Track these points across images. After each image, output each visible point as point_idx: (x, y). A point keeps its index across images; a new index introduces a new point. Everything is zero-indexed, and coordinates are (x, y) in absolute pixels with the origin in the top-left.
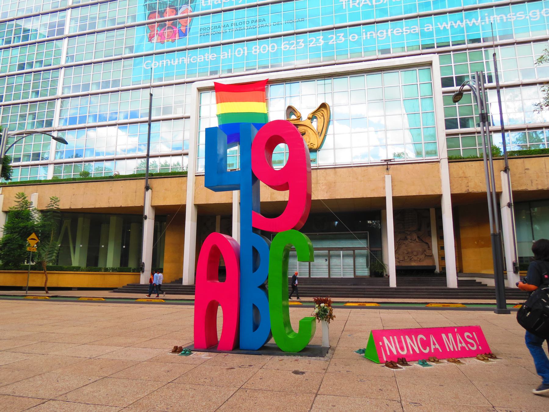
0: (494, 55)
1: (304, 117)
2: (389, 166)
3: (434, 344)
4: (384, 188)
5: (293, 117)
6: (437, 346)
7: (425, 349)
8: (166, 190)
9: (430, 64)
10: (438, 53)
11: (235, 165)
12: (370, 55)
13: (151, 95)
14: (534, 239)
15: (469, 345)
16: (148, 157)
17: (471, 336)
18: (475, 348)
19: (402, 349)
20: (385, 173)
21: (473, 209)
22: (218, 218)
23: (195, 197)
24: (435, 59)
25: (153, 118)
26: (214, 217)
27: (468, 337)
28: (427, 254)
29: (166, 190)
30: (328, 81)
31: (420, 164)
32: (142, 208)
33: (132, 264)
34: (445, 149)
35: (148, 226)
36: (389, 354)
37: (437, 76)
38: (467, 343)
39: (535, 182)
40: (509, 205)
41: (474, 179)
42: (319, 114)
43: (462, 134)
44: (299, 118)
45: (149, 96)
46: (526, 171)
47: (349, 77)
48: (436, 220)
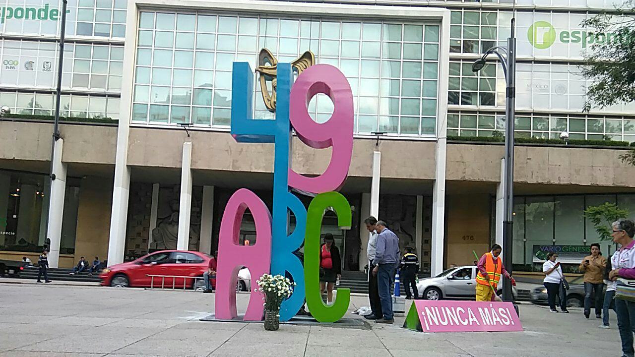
0: (513, 20)
2: (379, 141)
3: (472, 317)
4: (372, 167)
5: (267, 65)
6: (475, 319)
7: (464, 321)
9: (439, 20)
10: (448, 8)
11: (186, 119)
14: (525, 238)
15: (503, 320)
16: (59, 92)
17: (505, 312)
18: (508, 323)
19: (444, 321)
22: (156, 187)
24: (446, 14)
25: (66, 37)
27: (502, 312)
29: (85, 141)
30: (315, 24)
32: (49, 164)
35: (57, 190)
36: (431, 324)
37: (446, 40)
38: (501, 317)
39: (535, 174)
41: (481, 164)
42: (300, 66)
46: (528, 161)
47: (341, 21)
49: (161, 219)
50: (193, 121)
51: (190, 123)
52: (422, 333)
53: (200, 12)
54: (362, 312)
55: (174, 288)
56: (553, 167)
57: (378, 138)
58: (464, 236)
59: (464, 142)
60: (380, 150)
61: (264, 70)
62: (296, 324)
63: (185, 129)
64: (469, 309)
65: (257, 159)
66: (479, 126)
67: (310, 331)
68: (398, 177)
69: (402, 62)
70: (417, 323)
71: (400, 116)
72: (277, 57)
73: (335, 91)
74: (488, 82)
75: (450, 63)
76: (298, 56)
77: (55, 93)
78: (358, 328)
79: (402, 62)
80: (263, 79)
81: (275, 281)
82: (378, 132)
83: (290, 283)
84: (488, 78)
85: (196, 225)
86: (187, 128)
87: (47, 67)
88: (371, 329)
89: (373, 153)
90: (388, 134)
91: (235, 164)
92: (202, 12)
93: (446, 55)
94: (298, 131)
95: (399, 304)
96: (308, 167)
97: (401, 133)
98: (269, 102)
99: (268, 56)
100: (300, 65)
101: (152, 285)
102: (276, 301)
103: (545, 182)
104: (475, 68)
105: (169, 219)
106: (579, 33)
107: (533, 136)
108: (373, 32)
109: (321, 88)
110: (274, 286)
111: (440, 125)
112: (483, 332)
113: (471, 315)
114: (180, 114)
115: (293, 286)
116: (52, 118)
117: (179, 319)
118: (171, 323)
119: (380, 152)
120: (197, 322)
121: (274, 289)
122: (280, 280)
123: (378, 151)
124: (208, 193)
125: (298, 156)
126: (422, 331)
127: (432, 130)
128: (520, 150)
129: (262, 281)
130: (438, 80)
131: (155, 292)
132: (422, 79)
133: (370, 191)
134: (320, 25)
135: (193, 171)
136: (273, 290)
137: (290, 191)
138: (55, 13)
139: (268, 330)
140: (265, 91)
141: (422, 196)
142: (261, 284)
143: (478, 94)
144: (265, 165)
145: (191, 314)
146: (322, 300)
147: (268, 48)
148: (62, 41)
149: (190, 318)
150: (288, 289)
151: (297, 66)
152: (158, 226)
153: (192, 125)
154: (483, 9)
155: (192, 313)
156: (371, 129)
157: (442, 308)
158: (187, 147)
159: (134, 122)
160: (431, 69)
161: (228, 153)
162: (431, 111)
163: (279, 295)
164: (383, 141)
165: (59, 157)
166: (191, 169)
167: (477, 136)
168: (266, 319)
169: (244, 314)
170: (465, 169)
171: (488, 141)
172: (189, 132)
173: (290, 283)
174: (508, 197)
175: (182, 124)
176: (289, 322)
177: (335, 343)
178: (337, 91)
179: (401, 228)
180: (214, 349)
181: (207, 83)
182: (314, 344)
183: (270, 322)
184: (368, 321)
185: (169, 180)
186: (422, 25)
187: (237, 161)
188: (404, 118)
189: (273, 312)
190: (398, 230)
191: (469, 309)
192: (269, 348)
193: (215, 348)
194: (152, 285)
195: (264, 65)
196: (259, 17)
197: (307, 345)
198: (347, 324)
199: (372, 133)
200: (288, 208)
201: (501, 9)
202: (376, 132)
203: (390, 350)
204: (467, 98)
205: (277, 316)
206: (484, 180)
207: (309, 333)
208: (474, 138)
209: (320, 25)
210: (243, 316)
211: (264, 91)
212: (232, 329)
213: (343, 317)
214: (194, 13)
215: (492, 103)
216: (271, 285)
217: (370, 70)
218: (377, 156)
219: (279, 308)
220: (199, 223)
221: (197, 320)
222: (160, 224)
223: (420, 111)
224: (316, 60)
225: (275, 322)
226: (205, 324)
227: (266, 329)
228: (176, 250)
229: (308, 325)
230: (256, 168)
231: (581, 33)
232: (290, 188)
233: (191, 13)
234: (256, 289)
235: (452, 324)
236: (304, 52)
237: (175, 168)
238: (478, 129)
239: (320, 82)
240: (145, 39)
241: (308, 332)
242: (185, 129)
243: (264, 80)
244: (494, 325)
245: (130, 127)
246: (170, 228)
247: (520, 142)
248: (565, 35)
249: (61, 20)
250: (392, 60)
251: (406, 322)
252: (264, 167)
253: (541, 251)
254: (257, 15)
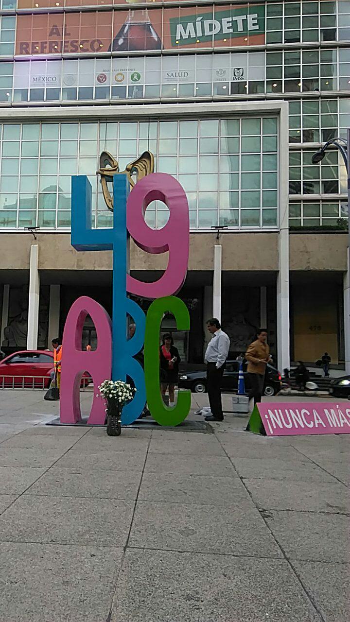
1: (122, 169)
2: (220, 234)
3: (318, 419)
4: (213, 261)
5: (108, 167)
6: (321, 421)
9: (277, 112)
10: (286, 99)
12: (83, 113)
19: (288, 424)
20: (215, 243)
22: (7, 287)
24: (284, 106)
30: (154, 125)
36: (275, 427)
42: (139, 166)
43: (305, 201)
44: (116, 168)
49: (12, 318)
50: (39, 224)
51: (37, 226)
52: (266, 437)
53: (43, 121)
54: (204, 413)
55: (23, 387)
57: (218, 233)
59: (308, 232)
60: (220, 243)
61: (105, 172)
62: (139, 428)
63: (32, 233)
64: (314, 411)
65: (99, 261)
66: (322, 214)
67: (151, 435)
68: (240, 270)
69: (240, 156)
70: (261, 427)
71: (240, 209)
72: (117, 159)
73: (169, 198)
74: (333, 170)
75: (289, 153)
78: (200, 432)
79: (240, 156)
81: (116, 388)
82: (218, 225)
83: (130, 388)
84: (332, 166)
85: (44, 323)
86: (34, 231)
88: (213, 433)
89: (214, 247)
90: (228, 228)
91: (79, 263)
92: (45, 121)
93: (285, 146)
94: (135, 239)
95: (243, 405)
96: (149, 263)
97: (241, 226)
98: (111, 202)
99: (108, 159)
100: (139, 165)
101: (3, 385)
102: (117, 406)
104: (315, 160)
105: (20, 317)
108: (211, 127)
109: (157, 195)
110: (115, 392)
111: (282, 216)
112: (329, 435)
113: (317, 417)
115: (134, 392)
117: (27, 424)
118: (20, 428)
119: (221, 246)
120: (43, 426)
121: (115, 395)
122: (121, 386)
123: (219, 244)
124: (55, 290)
125: (139, 253)
126: (265, 435)
127: (272, 221)
129: (103, 387)
131: (6, 392)
132: (261, 171)
133: (212, 284)
134: (158, 125)
135: (40, 272)
136: (114, 397)
137: (129, 296)
139: (111, 435)
140: (106, 192)
141: (266, 288)
142: (102, 390)
143: (321, 183)
144: (107, 263)
145: (38, 417)
146: (163, 402)
147: (108, 151)
149: (36, 422)
150: (128, 394)
151: (136, 167)
152: (9, 324)
153: (38, 229)
154: (323, 97)
155: (38, 416)
156: (212, 223)
157: (286, 411)
158: (34, 249)
160: (271, 159)
161: (73, 253)
162: (272, 201)
163: (120, 401)
164: (223, 234)
166: (38, 270)
167: (321, 225)
168: (108, 422)
169: (89, 416)
170: (309, 259)
171: (332, 230)
172: (35, 235)
173: (130, 388)
175: (29, 228)
176: (131, 426)
177: (176, 450)
178: (171, 198)
179: (245, 319)
180: (57, 458)
181: (52, 185)
182: (155, 451)
183: (113, 428)
184: (211, 423)
186: (260, 119)
187: (81, 261)
189: (114, 418)
190: (242, 322)
191: (314, 411)
192: (111, 457)
193: (59, 458)
194: (3, 385)
195: (105, 168)
196: (98, 122)
197: (147, 452)
198: (189, 427)
199: (212, 227)
200: (128, 315)
202: (216, 226)
203: (232, 458)
204: (309, 187)
205: (119, 421)
206: (330, 270)
207: (151, 438)
208: (318, 227)
209: (158, 125)
210: (86, 419)
211: (105, 192)
212: (76, 434)
213: (186, 419)
214: (38, 123)
216: (112, 391)
217: (209, 165)
218: (218, 249)
219: (120, 413)
220: (47, 321)
221: (43, 425)
222: (10, 323)
223: (260, 203)
224: (155, 158)
225: (117, 427)
226: (51, 428)
227: (109, 435)
228: (26, 349)
229: (149, 428)
230: (99, 267)
232: (128, 293)
233: (34, 123)
234: (97, 395)
235: (297, 427)
237: (24, 269)
238: (321, 218)
239: (155, 190)
241: (149, 437)
242: (32, 233)
243: (105, 181)
244: (341, 427)
246: (20, 326)
250: (232, 155)
251: (248, 425)
252: (107, 264)
254: (97, 120)
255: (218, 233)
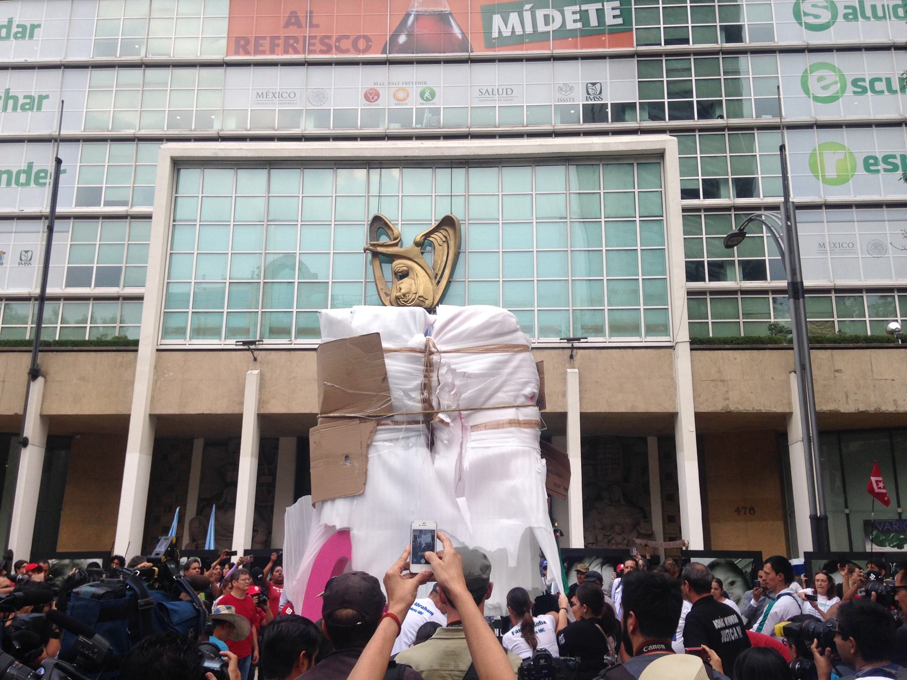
4: (564, 395)
5: (384, 239)
8: (82, 379)
9: (659, 156)
10: (673, 131)
11: (251, 333)
13: (59, 162)
14: (847, 507)
20: (567, 365)
21: (743, 449)
22: (199, 444)
23: (153, 397)
24: (669, 143)
25: (60, 210)
26: (644, 441)
28: (642, 531)
29: (82, 379)
30: (459, 173)
31: (635, 351)
33: (676, 113)
34: (686, 321)
37: (673, 177)
40: (25, 443)
41: (758, 384)
44: (397, 241)
45: (54, 164)
46: (837, 374)
48: (660, 462)
56: (882, 382)
58: (738, 508)
76: (433, 222)
77: (36, 299)
80: (377, 263)
86: (253, 347)
87: (25, 259)
89: (566, 373)
90: (590, 339)
93: (675, 203)
103: (872, 409)
104: (729, 243)
106: (894, 157)
107: (839, 331)
108: (554, 179)
114: (240, 322)
116: (28, 343)
119: (576, 370)
127: (663, 328)
128: (820, 358)
130: (666, 247)
132: (639, 248)
138: (42, 174)
148: (52, 219)
159: (164, 342)
162: (658, 295)
164: (581, 351)
165: (34, 410)
174: (809, 440)
185: (221, 434)
188: (615, 312)
201: (762, 128)
204: (712, 188)
208: (737, 339)
215: (739, 39)
231: (898, 157)
236: (443, 216)
240: (186, 209)
245: (158, 350)
247: (821, 342)
248: (871, 161)
249: (51, 186)
253: (878, 530)
255: (572, 348)
